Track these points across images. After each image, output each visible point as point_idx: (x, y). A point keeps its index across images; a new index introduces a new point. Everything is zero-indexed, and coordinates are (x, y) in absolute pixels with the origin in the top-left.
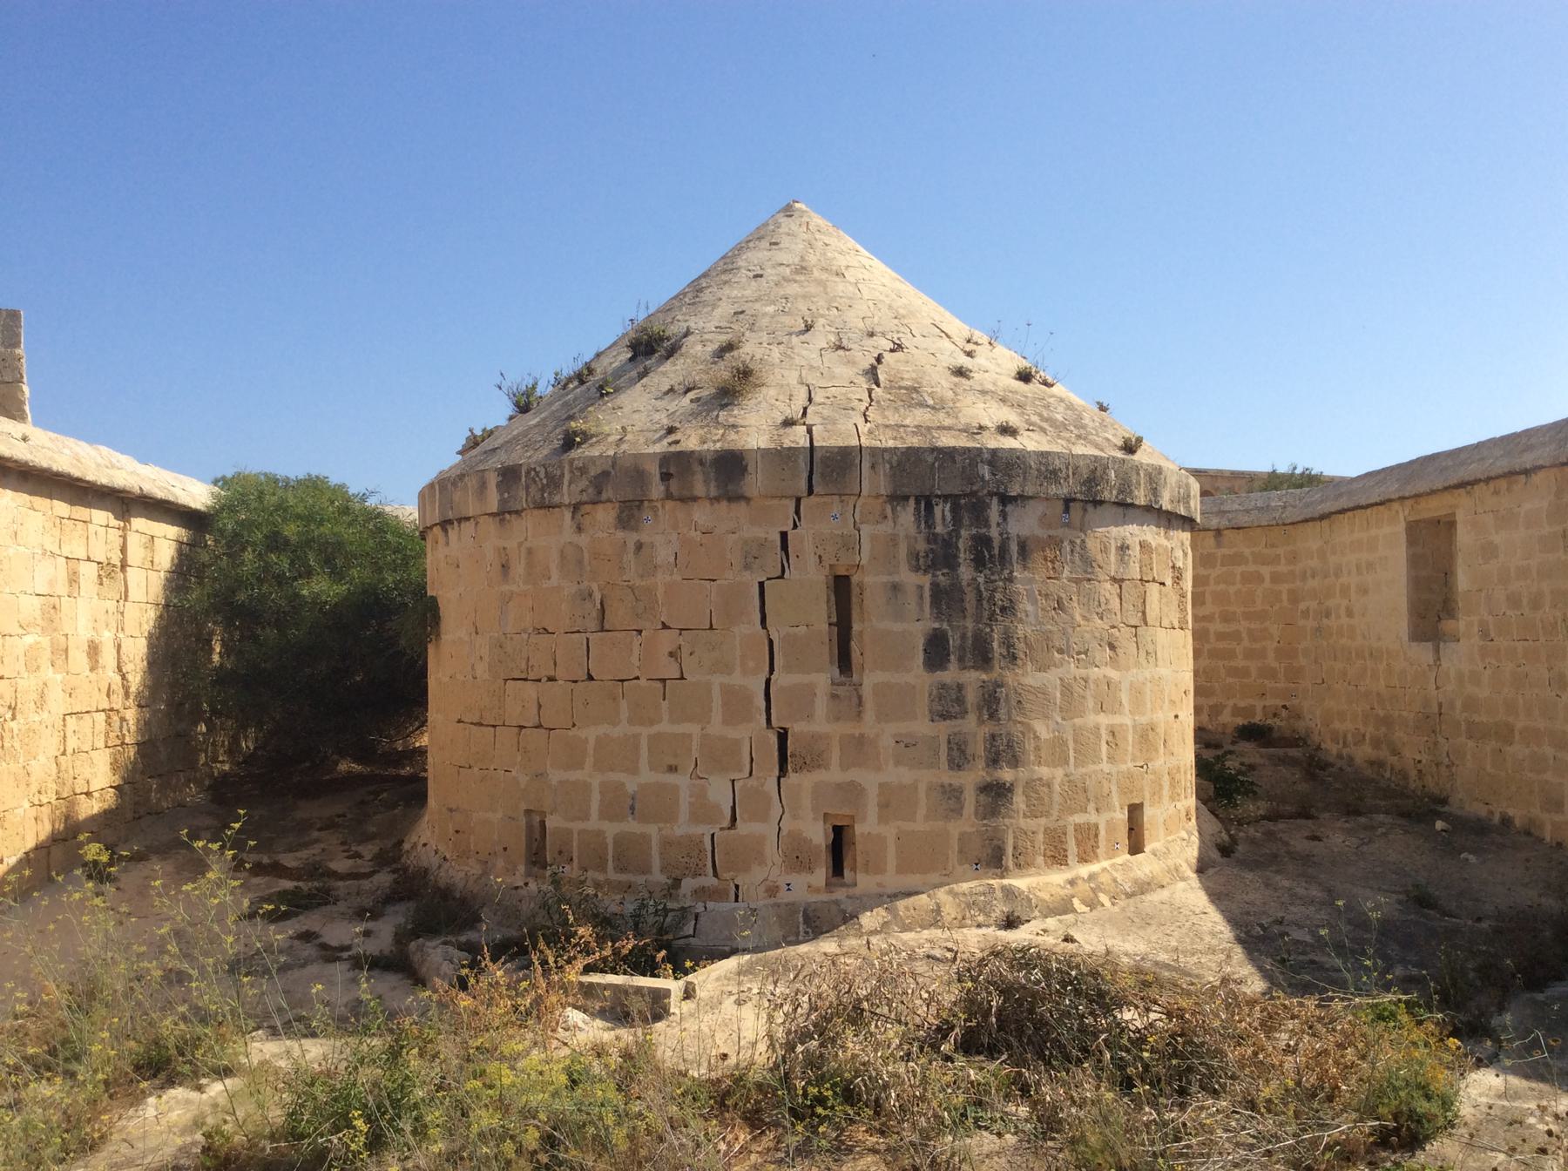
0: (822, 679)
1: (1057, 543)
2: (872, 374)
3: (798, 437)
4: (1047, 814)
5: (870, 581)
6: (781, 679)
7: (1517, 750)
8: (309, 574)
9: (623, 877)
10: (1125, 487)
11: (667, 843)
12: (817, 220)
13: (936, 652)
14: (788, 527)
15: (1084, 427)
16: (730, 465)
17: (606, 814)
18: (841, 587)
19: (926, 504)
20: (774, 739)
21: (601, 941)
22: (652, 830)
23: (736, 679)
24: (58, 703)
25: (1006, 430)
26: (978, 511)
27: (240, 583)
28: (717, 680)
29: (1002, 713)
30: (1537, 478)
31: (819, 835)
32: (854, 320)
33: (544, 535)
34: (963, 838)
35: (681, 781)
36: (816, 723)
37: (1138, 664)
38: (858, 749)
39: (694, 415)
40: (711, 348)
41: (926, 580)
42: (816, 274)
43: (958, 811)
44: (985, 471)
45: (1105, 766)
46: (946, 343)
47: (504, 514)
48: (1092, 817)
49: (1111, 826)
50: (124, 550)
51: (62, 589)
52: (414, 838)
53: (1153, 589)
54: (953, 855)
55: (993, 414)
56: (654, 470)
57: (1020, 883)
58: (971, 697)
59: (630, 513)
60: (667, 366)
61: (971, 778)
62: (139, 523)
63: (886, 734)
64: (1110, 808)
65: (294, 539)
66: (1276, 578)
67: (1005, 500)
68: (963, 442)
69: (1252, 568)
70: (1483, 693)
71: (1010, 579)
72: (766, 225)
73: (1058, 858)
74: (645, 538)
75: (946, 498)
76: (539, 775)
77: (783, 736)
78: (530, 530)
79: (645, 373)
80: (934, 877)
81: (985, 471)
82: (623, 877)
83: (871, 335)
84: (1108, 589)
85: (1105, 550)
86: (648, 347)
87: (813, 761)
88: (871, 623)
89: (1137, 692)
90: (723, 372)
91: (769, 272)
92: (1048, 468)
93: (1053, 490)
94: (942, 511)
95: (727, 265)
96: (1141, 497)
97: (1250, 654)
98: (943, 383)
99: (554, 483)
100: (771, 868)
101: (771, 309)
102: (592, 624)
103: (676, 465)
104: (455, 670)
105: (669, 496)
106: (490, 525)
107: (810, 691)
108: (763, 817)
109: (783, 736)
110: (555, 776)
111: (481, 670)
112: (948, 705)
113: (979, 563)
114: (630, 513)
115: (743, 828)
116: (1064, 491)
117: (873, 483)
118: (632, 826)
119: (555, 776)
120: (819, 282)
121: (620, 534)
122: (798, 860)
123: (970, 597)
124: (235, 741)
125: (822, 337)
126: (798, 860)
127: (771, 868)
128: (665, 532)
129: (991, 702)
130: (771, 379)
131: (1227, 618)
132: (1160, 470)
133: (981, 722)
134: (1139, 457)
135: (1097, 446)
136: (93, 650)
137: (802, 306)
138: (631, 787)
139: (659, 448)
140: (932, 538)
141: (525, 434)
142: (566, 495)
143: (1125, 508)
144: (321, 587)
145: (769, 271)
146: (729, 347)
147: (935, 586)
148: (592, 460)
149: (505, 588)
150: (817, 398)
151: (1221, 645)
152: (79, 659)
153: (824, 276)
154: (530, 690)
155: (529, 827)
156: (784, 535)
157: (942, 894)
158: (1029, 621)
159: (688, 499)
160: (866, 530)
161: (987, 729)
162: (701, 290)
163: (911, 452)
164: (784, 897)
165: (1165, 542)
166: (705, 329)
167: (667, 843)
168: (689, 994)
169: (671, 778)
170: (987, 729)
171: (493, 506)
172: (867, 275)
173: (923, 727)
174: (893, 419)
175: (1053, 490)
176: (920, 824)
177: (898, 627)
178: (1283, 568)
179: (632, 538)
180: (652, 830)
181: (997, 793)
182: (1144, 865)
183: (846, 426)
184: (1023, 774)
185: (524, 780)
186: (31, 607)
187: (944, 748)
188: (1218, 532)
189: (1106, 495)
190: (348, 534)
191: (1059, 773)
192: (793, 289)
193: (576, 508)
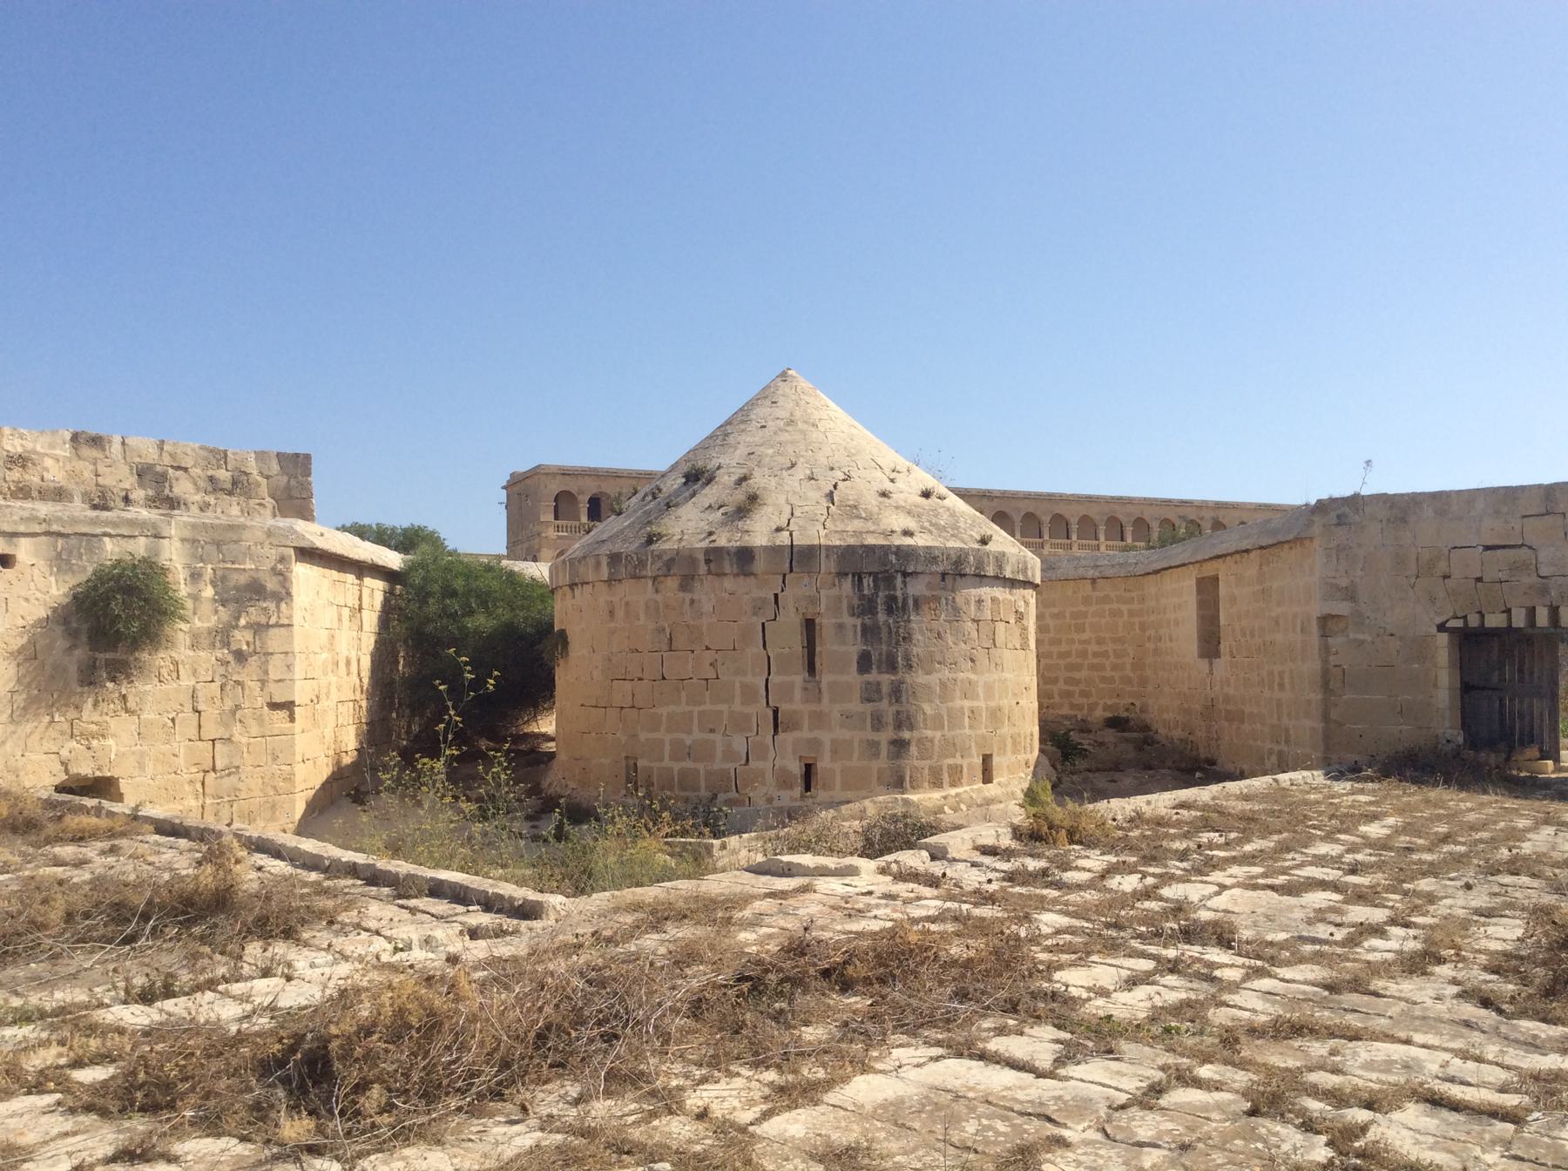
0: (798, 678)
1: (937, 599)
3: (784, 538)
4: (931, 758)
5: (826, 623)
7: (1246, 727)
8: (471, 613)
9: (683, 794)
10: (980, 564)
11: (709, 773)
12: (804, 384)
13: (864, 663)
15: (958, 528)
16: (745, 556)
17: (673, 758)
18: (810, 626)
20: (770, 713)
21: (675, 820)
22: (701, 767)
23: (749, 679)
24: (335, 696)
25: (907, 533)
26: (889, 580)
27: (429, 620)
28: (738, 680)
29: (904, 698)
30: (1253, 555)
31: (796, 769)
33: (637, 594)
35: (717, 738)
36: (794, 705)
37: (989, 671)
38: (819, 719)
39: (724, 524)
40: (734, 478)
41: (859, 622)
42: (800, 425)
43: (877, 755)
44: (893, 558)
45: (967, 731)
46: (879, 474)
48: (959, 761)
49: (970, 767)
50: (360, 599)
51: (335, 625)
52: (548, 781)
53: (1001, 626)
54: (874, 780)
55: (898, 522)
56: (701, 557)
57: (914, 797)
58: (885, 689)
59: (687, 583)
60: (707, 490)
62: (368, 581)
64: (970, 756)
65: (461, 590)
66: (1131, 614)
67: (905, 574)
68: (881, 541)
69: (1115, 606)
70: (1231, 691)
71: (909, 621)
72: (768, 387)
73: (937, 783)
74: (696, 597)
75: (870, 574)
76: (635, 736)
77: (776, 712)
78: (626, 590)
79: (694, 495)
80: (864, 793)
81: (893, 558)
82: (683, 794)
84: (969, 626)
85: (968, 603)
86: (696, 477)
87: (794, 725)
88: (827, 646)
89: (989, 688)
90: (740, 496)
92: (931, 556)
94: (868, 582)
95: (742, 416)
97: (1115, 667)
98: (871, 501)
99: (642, 563)
101: (770, 451)
102: (665, 647)
103: (714, 555)
104: (573, 675)
105: (710, 572)
106: (602, 587)
107: (792, 686)
108: (764, 758)
109: (776, 712)
110: (643, 736)
111: (597, 674)
112: (871, 694)
113: (890, 611)
114: (687, 583)
116: (940, 569)
117: (827, 566)
118: (688, 764)
120: (803, 432)
121: (681, 594)
122: (784, 782)
123: (884, 630)
124: (409, 726)
125: (801, 472)
126: (784, 782)
128: (707, 593)
129: (897, 692)
130: (769, 501)
131: (1100, 642)
132: (1004, 554)
133: (891, 704)
134: (991, 547)
136: (348, 663)
138: (688, 742)
139: (705, 544)
140: (862, 597)
141: (622, 532)
143: (980, 578)
144: (481, 622)
145: (770, 423)
146: (744, 479)
148: (665, 551)
149: (612, 625)
150: (797, 513)
151: (1096, 661)
152: (342, 665)
153: (805, 427)
154: (628, 686)
155: (627, 767)
156: (776, 596)
157: (867, 803)
158: (920, 644)
159: (721, 575)
161: (894, 708)
162: (727, 435)
164: (776, 803)
165: (1008, 597)
166: (729, 463)
167: (709, 773)
168: (723, 847)
169: (711, 736)
170: (894, 708)
171: (605, 576)
172: (832, 425)
173: (856, 706)
176: (855, 762)
178: (1136, 606)
179: (688, 596)
180: (701, 767)
181: (900, 746)
182: (991, 790)
183: (813, 534)
184: (916, 734)
185: (624, 739)
186: (324, 635)
187: (869, 720)
188: (1094, 581)
189: (968, 570)
190: (495, 584)
191: (938, 734)
192: (785, 437)
193: (655, 579)
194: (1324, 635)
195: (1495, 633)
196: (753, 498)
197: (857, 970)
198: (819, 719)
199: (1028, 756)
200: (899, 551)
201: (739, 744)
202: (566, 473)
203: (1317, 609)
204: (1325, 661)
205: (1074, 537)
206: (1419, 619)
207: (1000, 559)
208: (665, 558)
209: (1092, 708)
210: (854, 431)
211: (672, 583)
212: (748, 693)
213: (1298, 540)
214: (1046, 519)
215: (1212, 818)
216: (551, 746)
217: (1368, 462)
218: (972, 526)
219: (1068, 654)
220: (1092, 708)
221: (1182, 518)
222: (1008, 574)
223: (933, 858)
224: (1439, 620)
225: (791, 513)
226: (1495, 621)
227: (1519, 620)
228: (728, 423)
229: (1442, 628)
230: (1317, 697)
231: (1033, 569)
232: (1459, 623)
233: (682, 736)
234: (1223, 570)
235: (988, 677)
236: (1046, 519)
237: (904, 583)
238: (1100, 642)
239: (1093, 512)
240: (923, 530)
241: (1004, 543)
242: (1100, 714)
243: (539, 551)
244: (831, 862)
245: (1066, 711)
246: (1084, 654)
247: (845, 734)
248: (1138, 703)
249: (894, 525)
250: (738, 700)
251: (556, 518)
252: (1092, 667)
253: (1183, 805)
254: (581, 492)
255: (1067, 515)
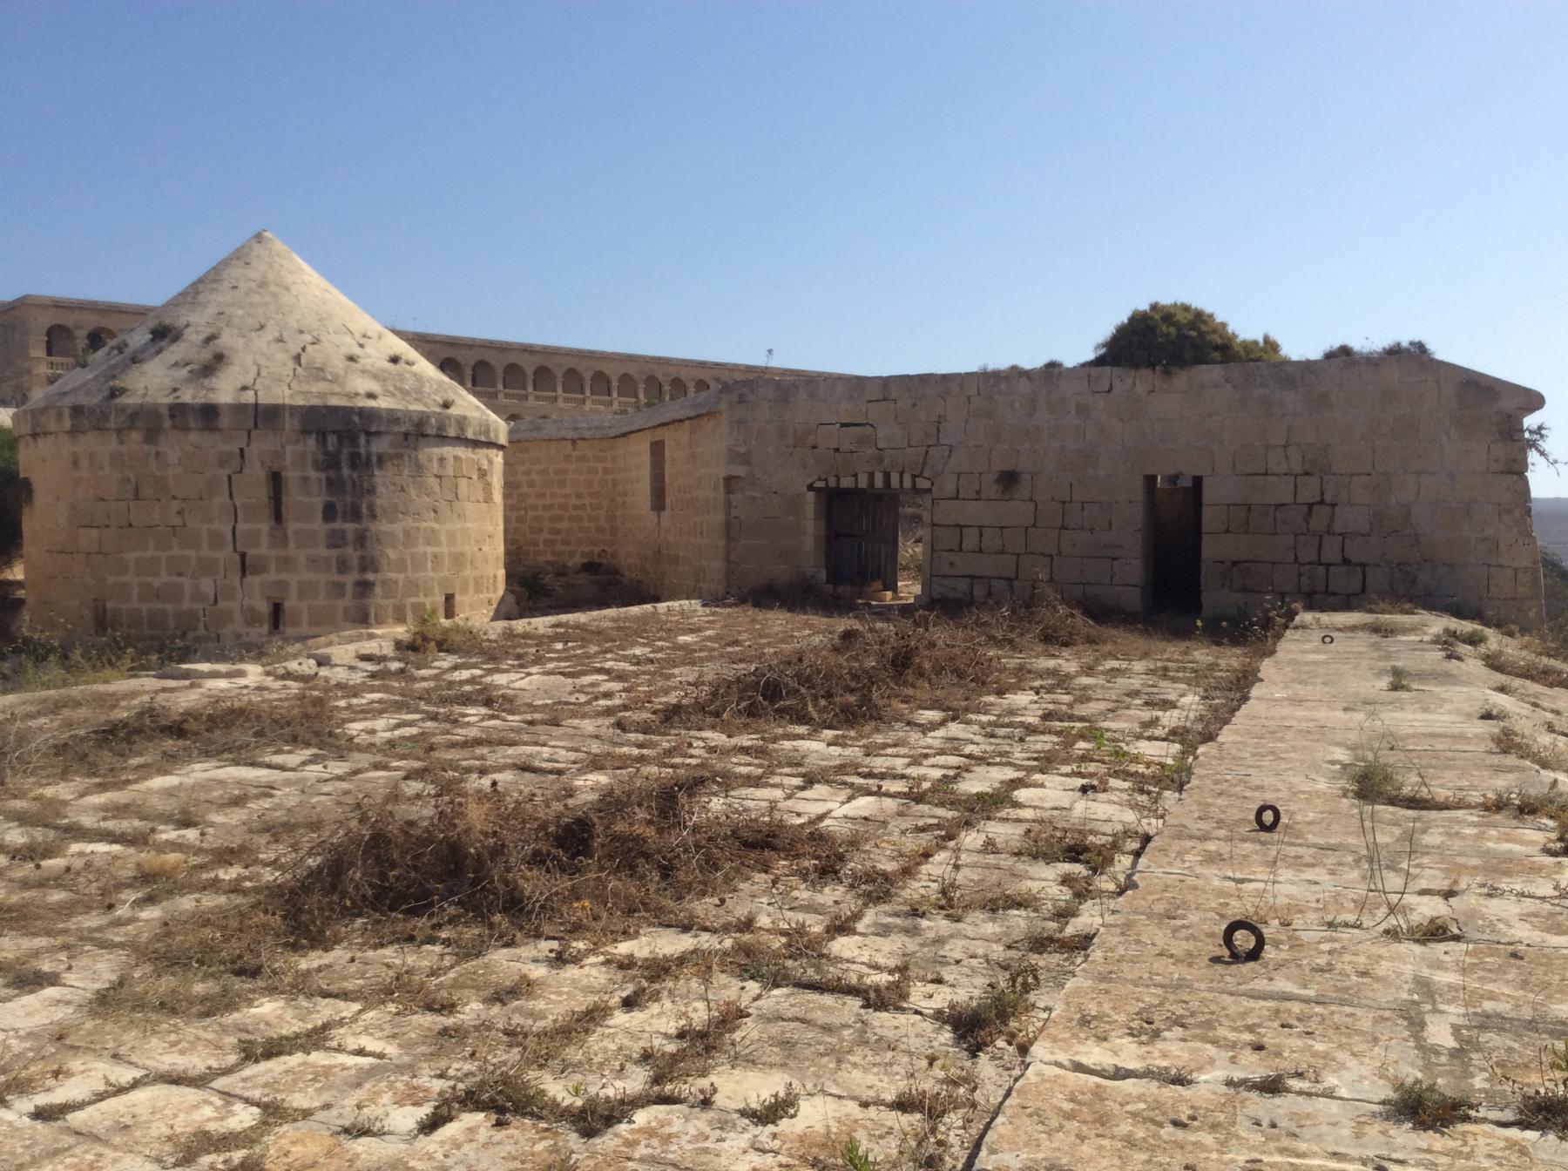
0: (264, 527)
2: (297, 359)
3: (248, 397)
5: (291, 475)
6: (241, 527)
10: (441, 426)
12: (279, 246)
13: (329, 513)
14: (243, 445)
16: (209, 413)
18: (276, 479)
19: (322, 436)
20: (237, 558)
22: (169, 607)
25: (371, 396)
26: (354, 440)
28: (205, 528)
29: (368, 543)
31: (263, 607)
32: (292, 322)
33: (100, 446)
34: (345, 609)
35: (185, 581)
36: (263, 550)
38: (286, 563)
39: (189, 381)
40: (202, 337)
41: (323, 476)
42: (273, 288)
43: (343, 595)
44: (356, 419)
45: (430, 574)
46: (348, 339)
47: (74, 432)
53: (463, 483)
55: (363, 384)
56: (165, 412)
58: (350, 536)
59: (152, 435)
60: (174, 347)
61: (350, 579)
63: (301, 555)
66: (605, 471)
67: (368, 434)
68: (344, 403)
69: (592, 464)
71: (373, 475)
72: (243, 247)
74: (161, 448)
75: (333, 432)
77: (243, 556)
78: (89, 442)
79: (159, 351)
81: (356, 419)
83: (301, 332)
85: (430, 460)
87: (260, 568)
88: (294, 497)
89: (452, 537)
90: (206, 355)
91: (243, 286)
92: (393, 417)
93: (396, 429)
94: (332, 440)
95: (212, 277)
96: (452, 432)
98: (338, 364)
99: (105, 416)
100: (238, 625)
101: (240, 312)
103: (178, 411)
109: (243, 556)
112: (336, 540)
113: (353, 467)
114: (152, 435)
115: (222, 605)
116: (403, 429)
117: (290, 424)
118: (158, 605)
119: (111, 579)
120: (275, 295)
125: (270, 334)
127: (238, 625)
128: (173, 447)
129: (361, 539)
131: (579, 496)
132: (465, 418)
134: (453, 411)
135: (426, 405)
137: (260, 311)
140: (326, 453)
141: (85, 384)
142: (113, 422)
143: (442, 438)
147: (328, 479)
150: (263, 373)
154: (94, 533)
156: (242, 450)
158: (384, 497)
160: (289, 449)
161: (358, 553)
162: (198, 293)
163: (312, 408)
166: (198, 322)
170: (358, 553)
173: (322, 551)
174: (305, 388)
175: (396, 429)
176: (322, 601)
177: (307, 500)
178: (609, 465)
179: (153, 449)
180: (169, 607)
181: (364, 587)
183: (281, 394)
184: (380, 576)
188: (574, 441)
191: (401, 577)
192: (256, 298)
194: (729, 492)
195: (854, 493)
196: (219, 358)
197: (192, 726)
198: (286, 563)
199: (492, 595)
200: (361, 412)
201: (207, 586)
202: (59, 305)
203: (723, 471)
204: (728, 514)
205: (615, 394)
206: (794, 479)
207: (462, 422)
208: (129, 411)
209: (572, 554)
210: (327, 296)
211: (136, 436)
212: (216, 541)
213: (711, 414)
214: (588, 375)
215: (587, 635)
216: (21, 593)
217: (770, 351)
218: (437, 392)
219: (551, 507)
220: (572, 554)
221: (717, 380)
222: (470, 435)
223: (319, 664)
224: (809, 481)
225: (257, 373)
226: (847, 483)
227: (863, 483)
228: (200, 281)
229: (810, 487)
230: (722, 543)
231: (496, 431)
232: (821, 484)
233: (150, 579)
234: (665, 434)
235: (449, 526)
236: (588, 375)
237: (368, 442)
238: (579, 496)
239: (633, 370)
240: (387, 393)
241: (468, 405)
242: (578, 559)
243: (29, 389)
244: (222, 667)
245: (550, 558)
246: (564, 507)
247: (309, 576)
248: (609, 550)
249: (360, 388)
250: (205, 545)
251: (50, 353)
252: (572, 518)
253: (558, 625)
254: (79, 327)
255: (608, 373)
